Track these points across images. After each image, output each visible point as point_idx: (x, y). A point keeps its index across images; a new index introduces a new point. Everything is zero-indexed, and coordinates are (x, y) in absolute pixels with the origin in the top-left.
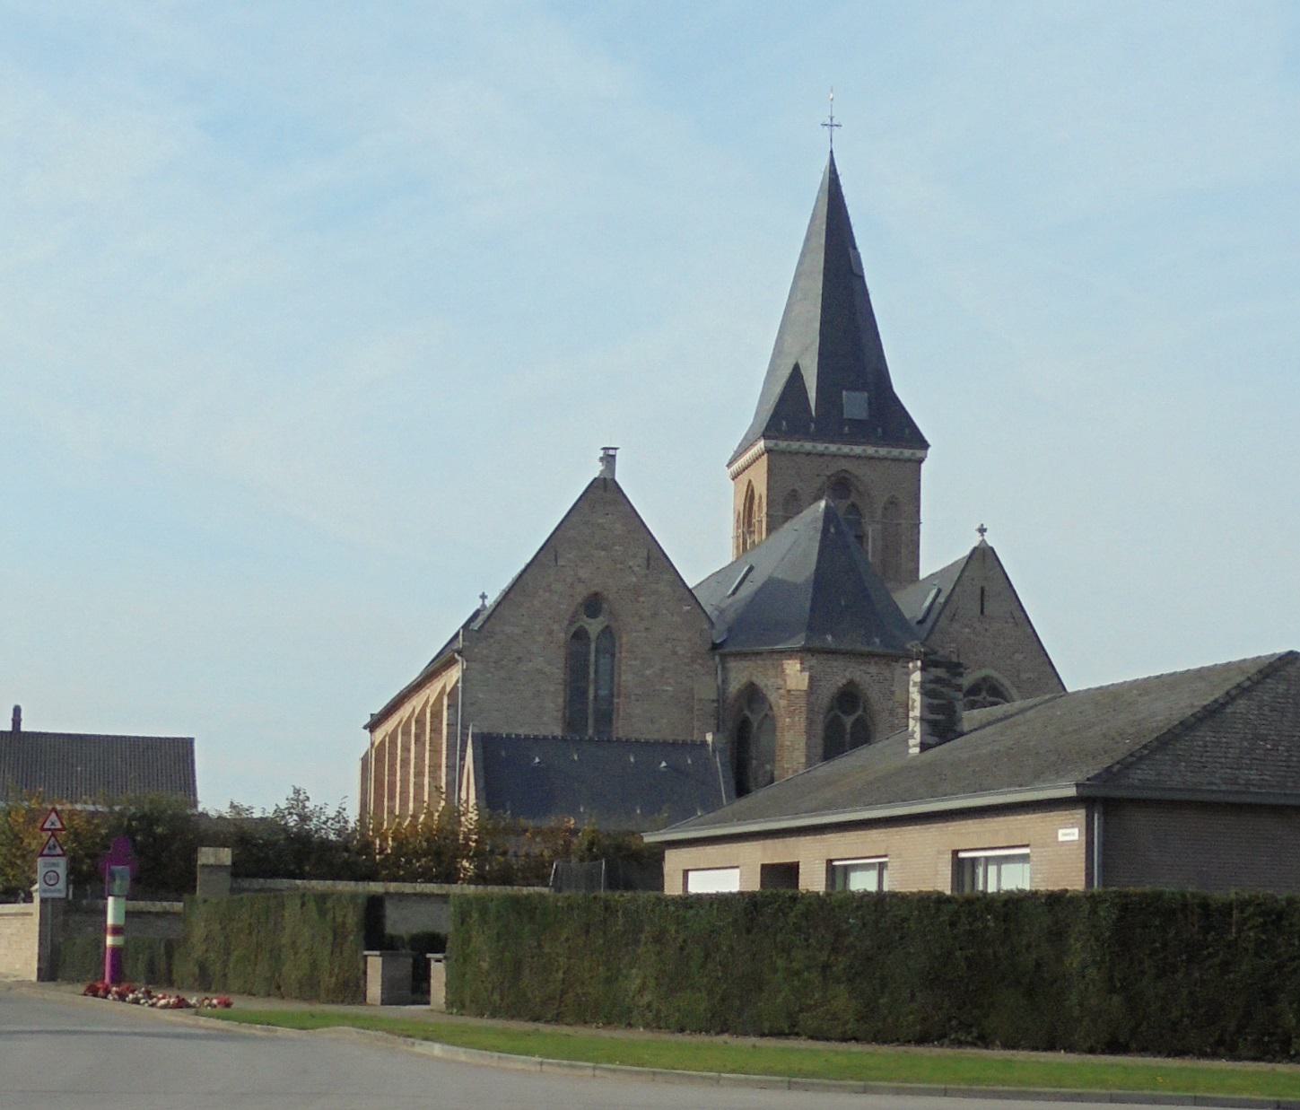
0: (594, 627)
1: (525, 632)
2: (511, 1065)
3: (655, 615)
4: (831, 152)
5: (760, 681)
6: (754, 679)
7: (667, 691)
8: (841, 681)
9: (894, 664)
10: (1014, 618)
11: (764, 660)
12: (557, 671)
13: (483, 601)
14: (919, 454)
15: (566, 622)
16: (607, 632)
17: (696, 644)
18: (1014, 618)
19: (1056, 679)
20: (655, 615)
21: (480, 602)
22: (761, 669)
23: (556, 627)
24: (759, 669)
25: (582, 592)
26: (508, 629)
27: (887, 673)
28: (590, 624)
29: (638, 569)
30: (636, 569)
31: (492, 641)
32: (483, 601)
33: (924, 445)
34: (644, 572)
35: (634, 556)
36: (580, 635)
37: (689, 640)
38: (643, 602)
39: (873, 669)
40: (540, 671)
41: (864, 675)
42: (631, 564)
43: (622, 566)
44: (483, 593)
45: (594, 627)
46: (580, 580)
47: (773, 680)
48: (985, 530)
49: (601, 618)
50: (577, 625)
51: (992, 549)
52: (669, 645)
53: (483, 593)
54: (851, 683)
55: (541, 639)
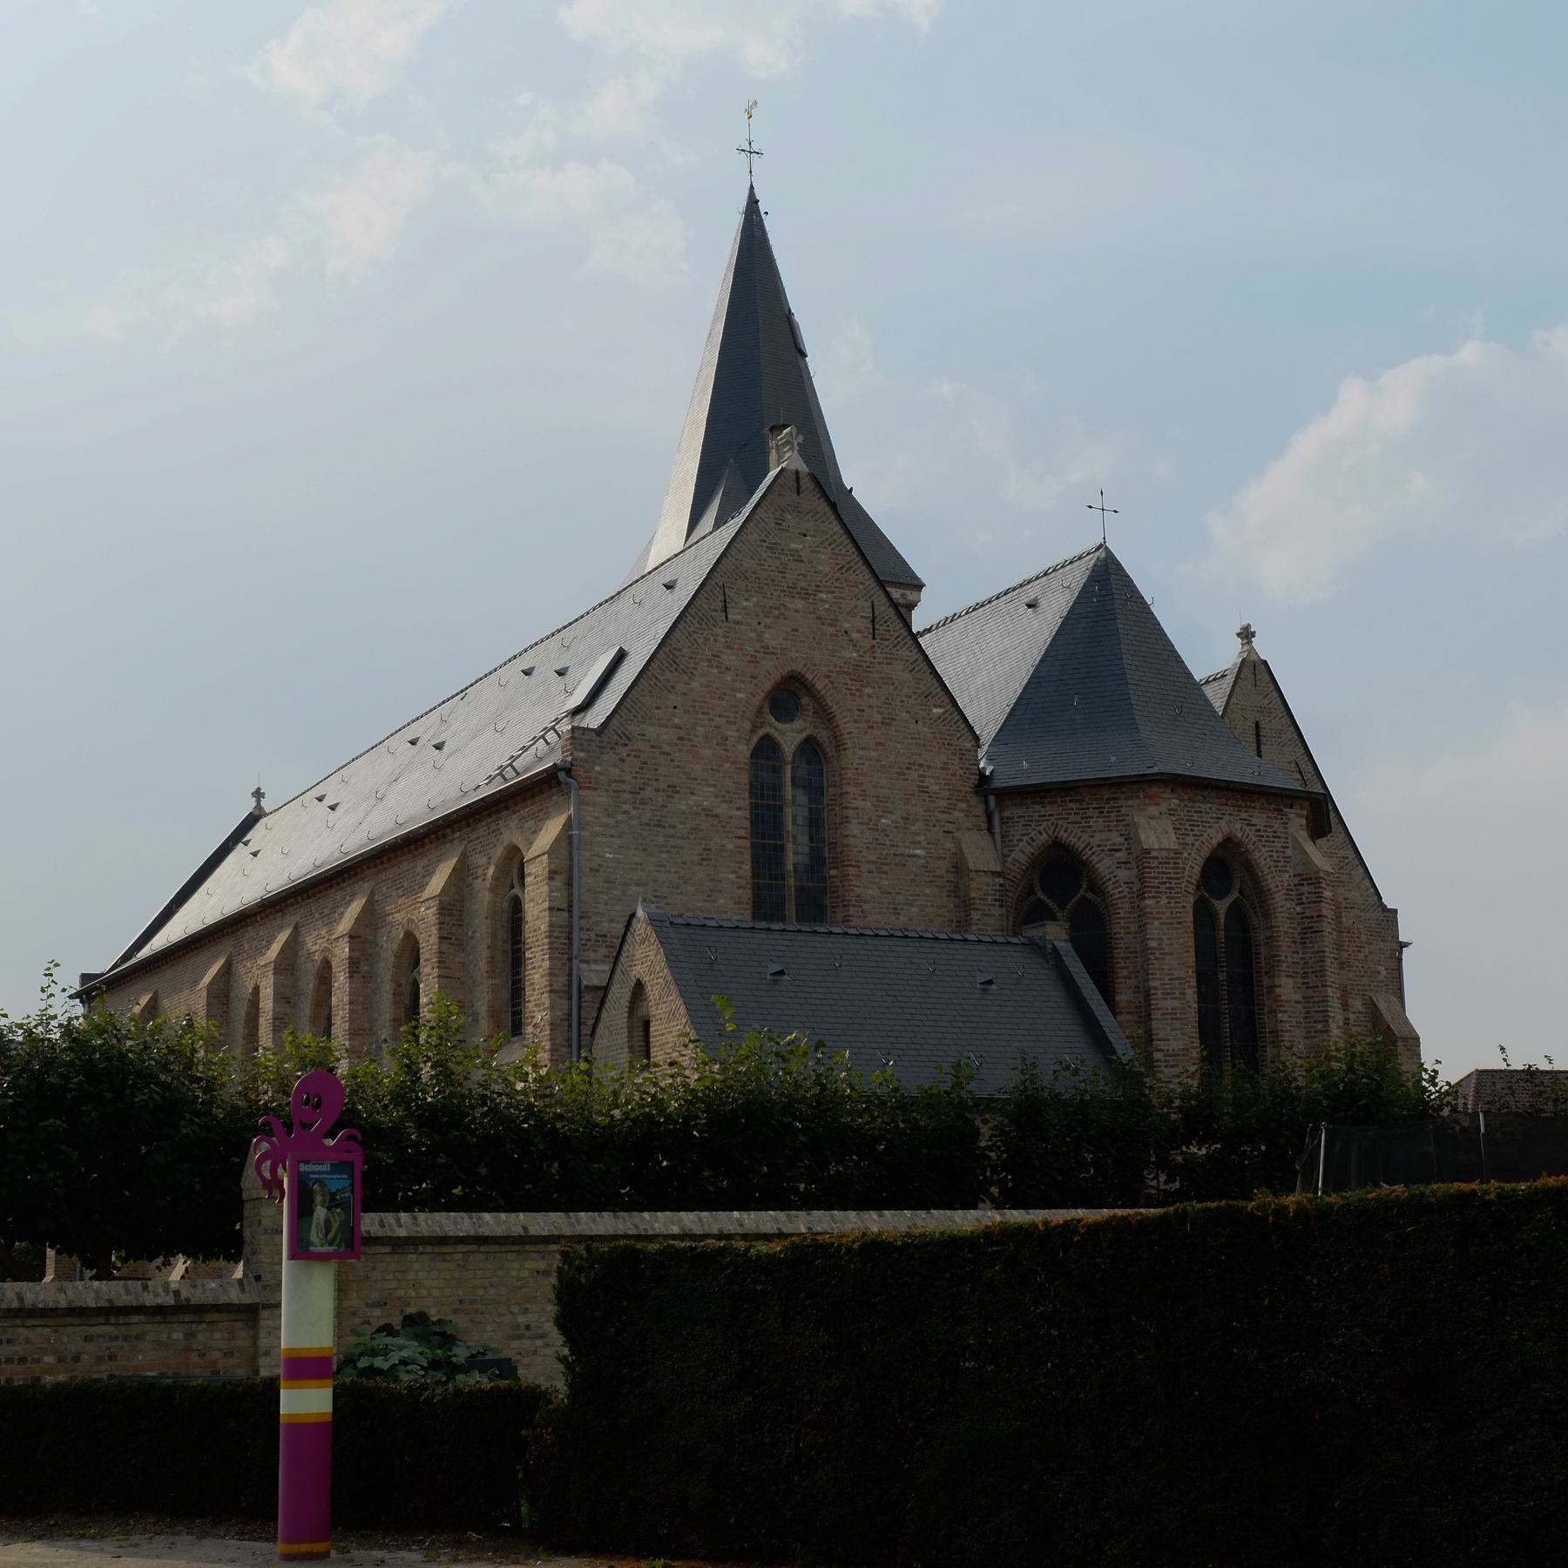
0: (790, 736)
1: (681, 739)
2: (397, 1556)
3: (888, 722)
4: (752, 187)
5: (1074, 837)
6: (1063, 835)
7: (915, 856)
8: (1213, 836)
9: (1287, 810)
10: (1301, 773)
11: (1081, 801)
12: (738, 814)
13: (258, 802)
14: (911, 596)
15: (748, 726)
16: (810, 747)
17: (954, 774)
18: (1301, 773)
19: (1361, 870)
20: (888, 722)
21: (252, 803)
22: (1078, 818)
23: (731, 733)
24: (1072, 818)
25: (770, 673)
26: (651, 731)
27: (1277, 825)
28: (782, 733)
29: (859, 636)
30: (855, 636)
31: (623, 751)
32: (258, 802)
33: (918, 586)
34: (868, 643)
35: (852, 612)
36: (766, 749)
37: (945, 768)
38: (869, 696)
39: (1259, 820)
40: (709, 813)
41: (1247, 828)
42: (847, 626)
43: (832, 630)
44: (259, 789)
45: (790, 736)
46: (767, 650)
47: (1104, 835)
48: (1253, 634)
49: (798, 724)
50: (761, 732)
51: (1265, 663)
52: (914, 775)
53: (259, 789)
54: (1228, 842)
55: (707, 752)
